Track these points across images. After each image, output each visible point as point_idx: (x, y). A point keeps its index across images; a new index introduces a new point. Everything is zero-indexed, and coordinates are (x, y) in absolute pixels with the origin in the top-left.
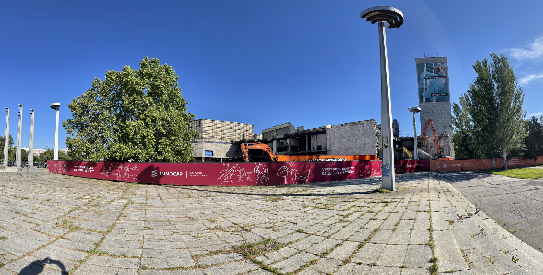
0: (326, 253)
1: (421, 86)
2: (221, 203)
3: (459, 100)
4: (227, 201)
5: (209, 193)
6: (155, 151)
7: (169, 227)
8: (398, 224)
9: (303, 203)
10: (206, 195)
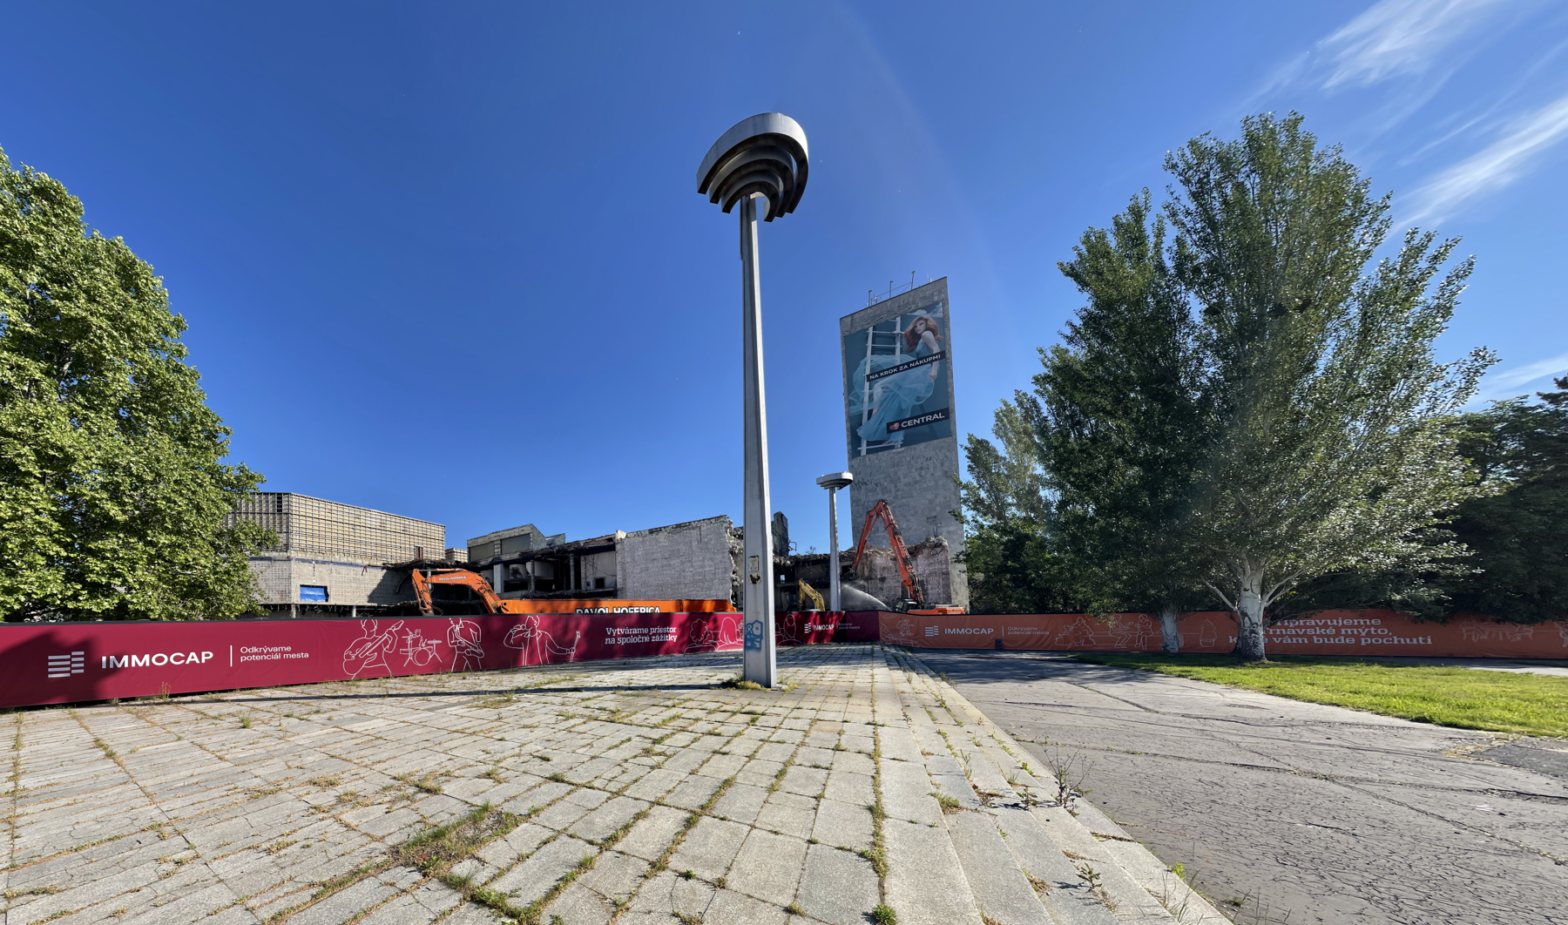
0: (613, 839)
2: (356, 727)
3: (993, 420)
4: (374, 717)
5: (315, 703)
6: (68, 579)
7: (157, 848)
8: (781, 774)
9: (563, 708)
10: (304, 709)
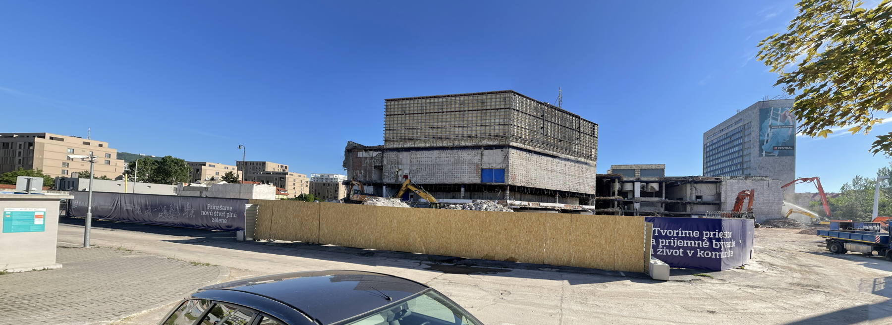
1: (761, 138)
